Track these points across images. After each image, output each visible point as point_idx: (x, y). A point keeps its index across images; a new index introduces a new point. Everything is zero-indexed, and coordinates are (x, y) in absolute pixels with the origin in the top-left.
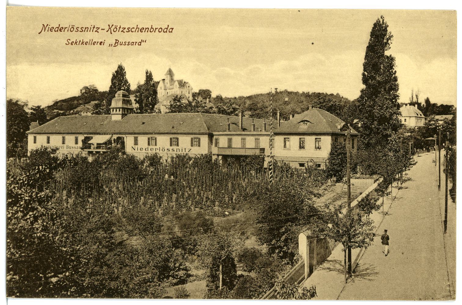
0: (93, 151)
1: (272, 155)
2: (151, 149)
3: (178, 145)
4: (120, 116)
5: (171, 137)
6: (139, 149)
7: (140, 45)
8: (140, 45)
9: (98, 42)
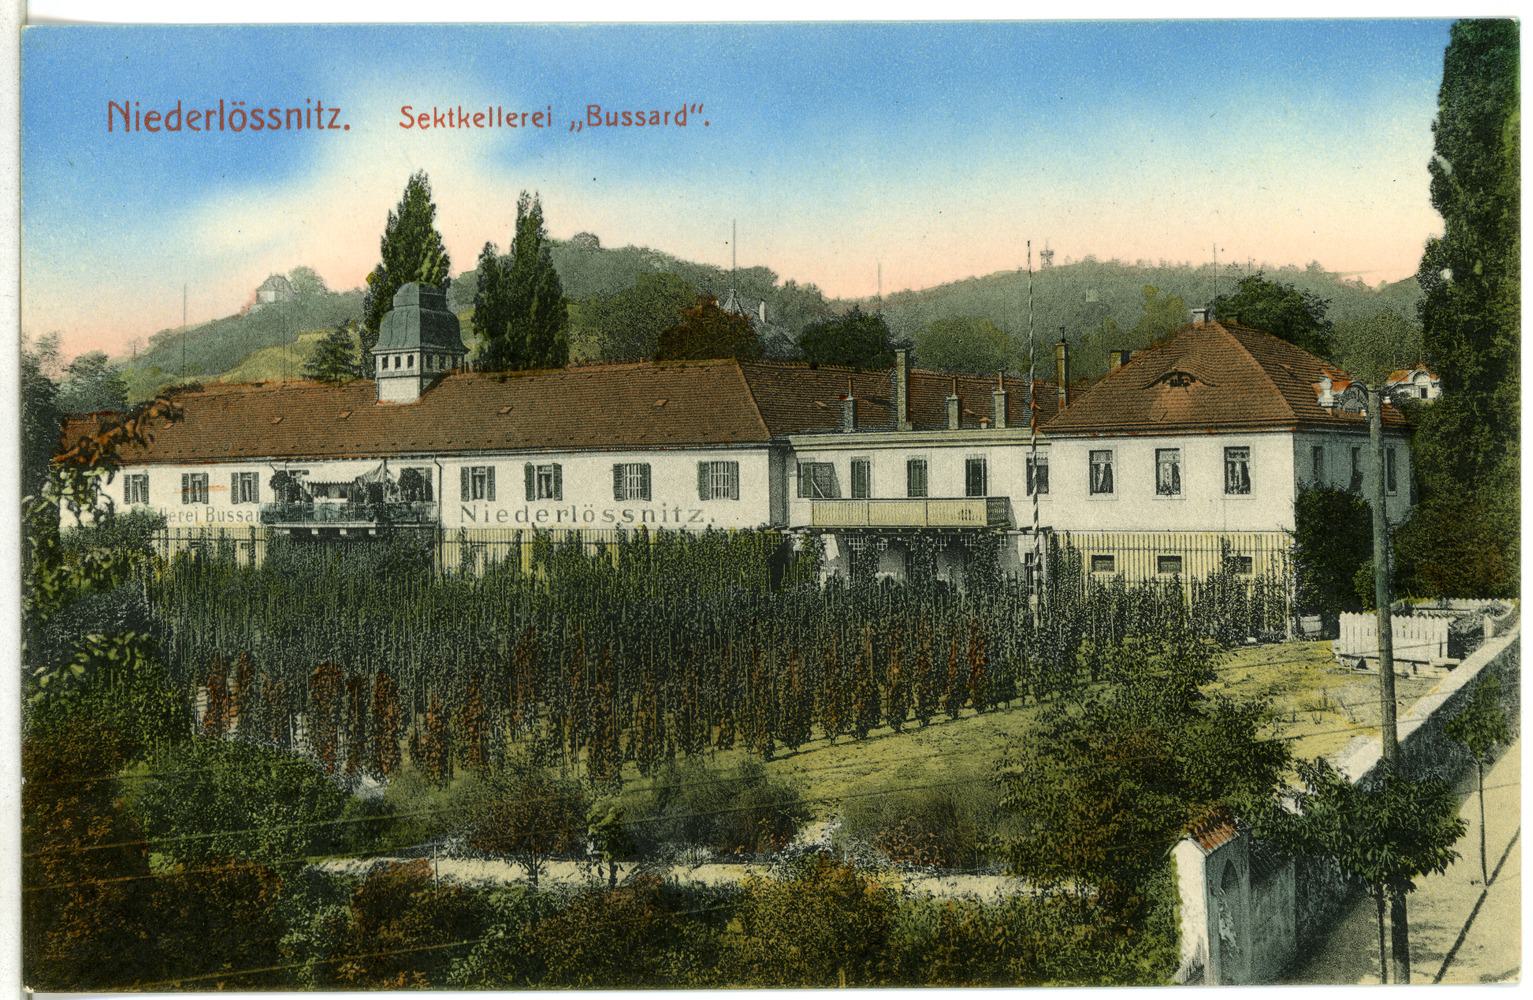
0: (338, 529)
1: (1043, 523)
2: (498, 516)
3: (492, 497)
4: (414, 383)
5: (465, 465)
6: (492, 518)
7: (684, 123)
8: (684, 123)
9: (524, 115)
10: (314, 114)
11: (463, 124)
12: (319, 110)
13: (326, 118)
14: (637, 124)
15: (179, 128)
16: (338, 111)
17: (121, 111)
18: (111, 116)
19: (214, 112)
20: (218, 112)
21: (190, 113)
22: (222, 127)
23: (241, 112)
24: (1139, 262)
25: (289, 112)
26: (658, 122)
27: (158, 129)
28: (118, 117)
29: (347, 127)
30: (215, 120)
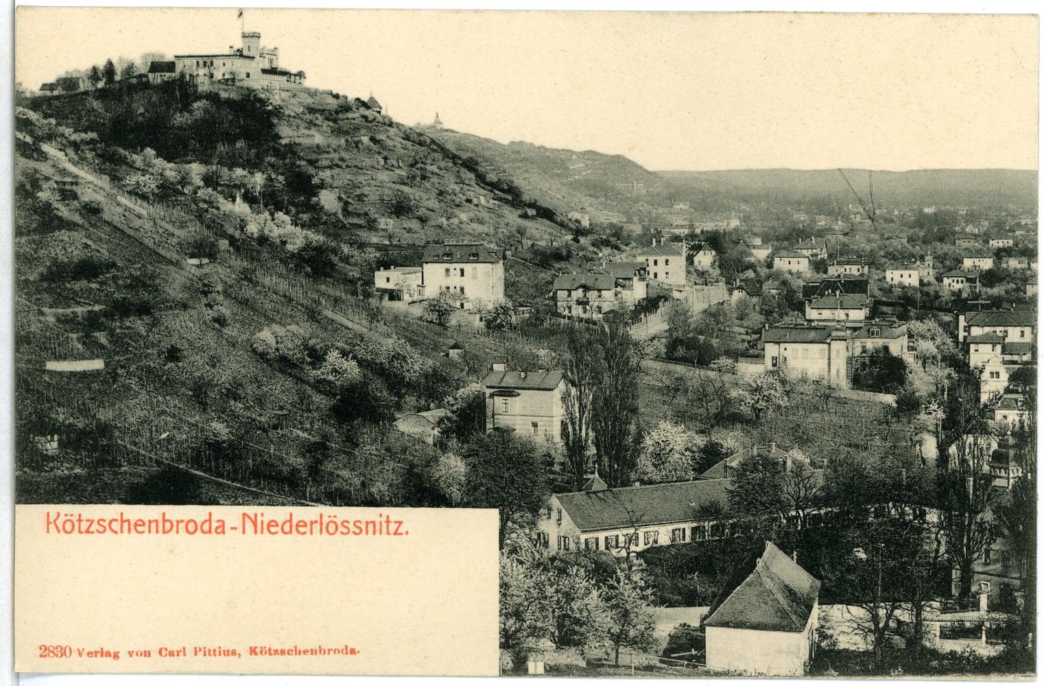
10: (384, 525)
11: (52, 527)
12: (388, 522)
13: (393, 527)
14: (354, 533)
15: (291, 532)
16: (400, 523)
17: (251, 519)
18: (244, 523)
19: (116, 520)
20: (319, 520)
21: (272, 521)
22: (321, 532)
23: (335, 523)
24: (67, 72)
25: (367, 523)
26: (223, 532)
27: (305, 533)
28: (249, 526)
29: (407, 533)
30: (316, 527)
